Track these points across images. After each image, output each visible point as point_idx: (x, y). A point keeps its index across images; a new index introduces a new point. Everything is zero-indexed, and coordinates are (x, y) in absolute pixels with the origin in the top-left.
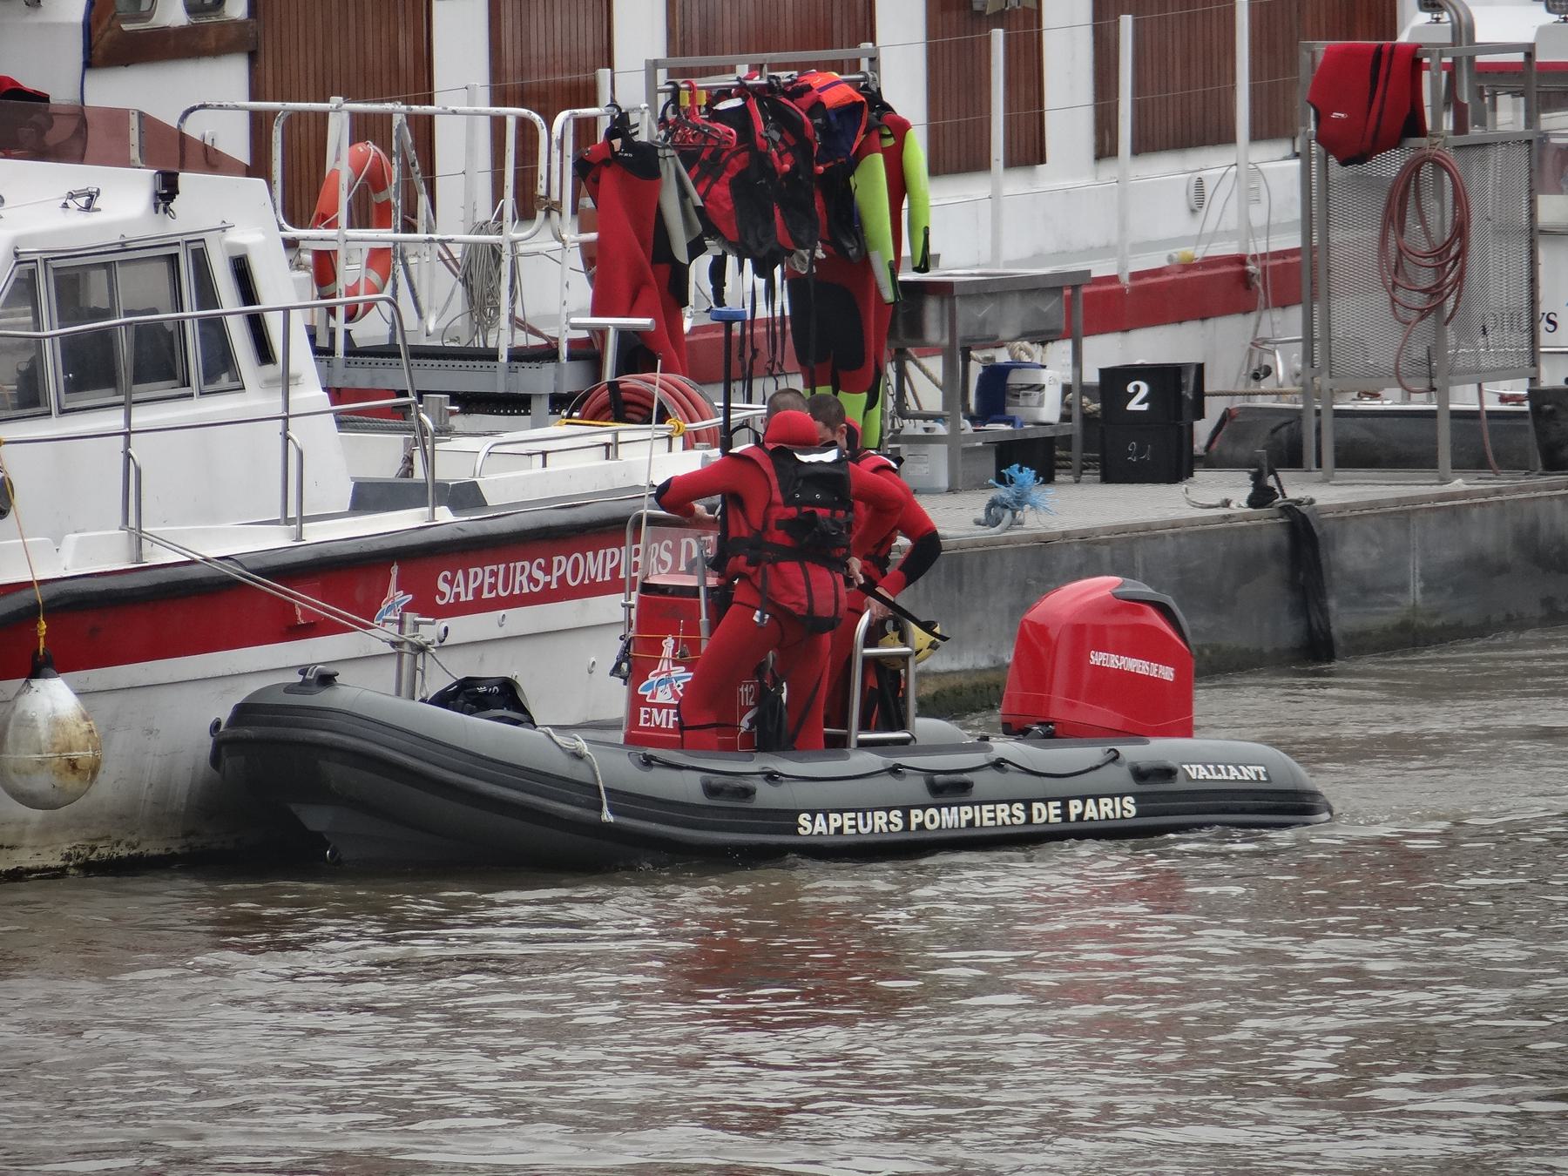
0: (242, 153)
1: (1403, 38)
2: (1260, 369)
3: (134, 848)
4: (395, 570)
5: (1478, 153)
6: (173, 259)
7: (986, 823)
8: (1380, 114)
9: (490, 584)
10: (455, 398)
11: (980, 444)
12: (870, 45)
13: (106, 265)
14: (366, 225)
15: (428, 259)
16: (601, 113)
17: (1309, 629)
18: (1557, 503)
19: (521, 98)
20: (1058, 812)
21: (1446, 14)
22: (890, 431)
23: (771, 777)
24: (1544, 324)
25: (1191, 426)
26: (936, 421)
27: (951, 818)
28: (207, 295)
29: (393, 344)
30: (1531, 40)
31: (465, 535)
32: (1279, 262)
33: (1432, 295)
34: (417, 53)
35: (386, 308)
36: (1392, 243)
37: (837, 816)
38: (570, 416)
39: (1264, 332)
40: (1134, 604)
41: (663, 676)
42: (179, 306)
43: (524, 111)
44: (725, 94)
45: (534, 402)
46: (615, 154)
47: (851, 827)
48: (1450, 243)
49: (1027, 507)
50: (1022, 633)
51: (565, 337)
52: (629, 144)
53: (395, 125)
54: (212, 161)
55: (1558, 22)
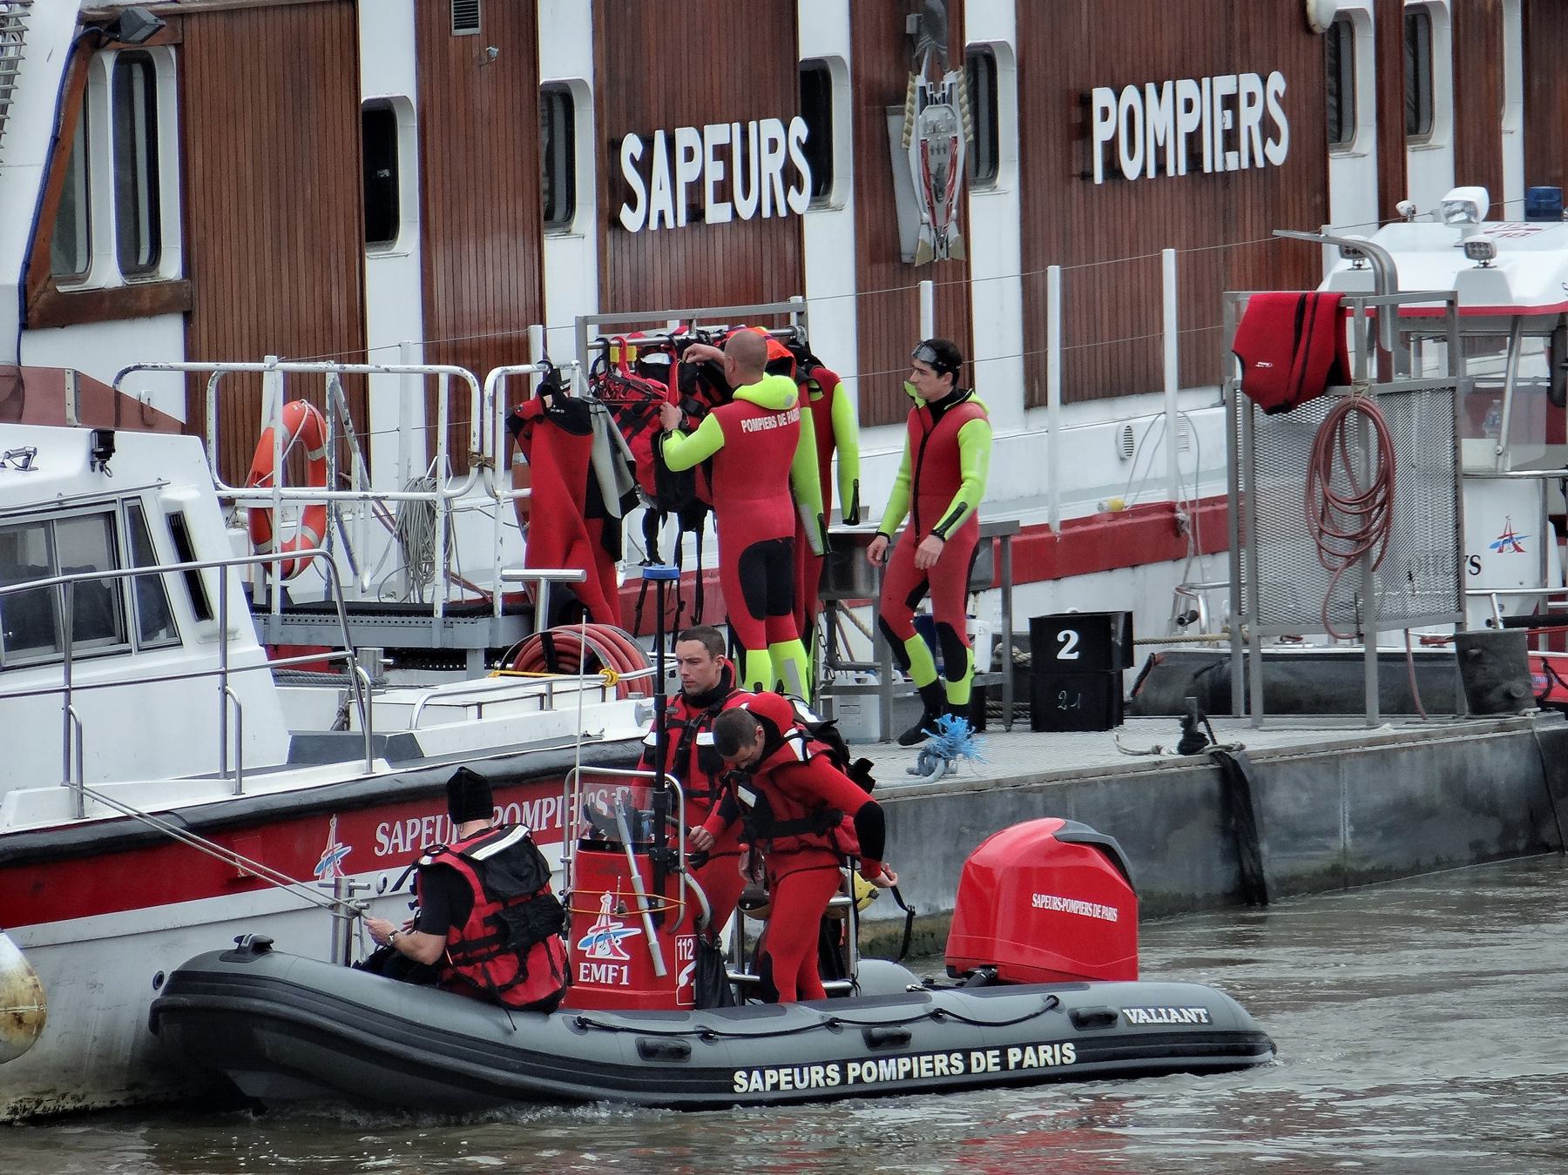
0: (178, 412)
1: (1324, 288)
2: (1186, 614)
3: (79, 1101)
4: (334, 822)
5: (1402, 400)
6: (110, 516)
7: (924, 1074)
8: (1305, 363)
9: (428, 835)
10: (388, 652)
11: (911, 694)
12: (800, 298)
13: (43, 524)
14: (302, 483)
15: (362, 515)
16: (534, 371)
17: (1242, 874)
18: (1485, 746)
19: (454, 355)
20: (997, 1060)
21: (1367, 260)
22: (823, 682)
23: (706, 1036)
24: (1468, 566)
25: (1121, 674)
26: (867, 672)
27: (890, 1070)
28: (144, 552)
29: (329, 601)
30: (1451, 288)
31: (403, 786)
32: (1210, 508)
33: (1359, 541)
34: (350, 311)
35: (321, 562)
36: (1318, 490)
37: (774, 1072)
38: (503, 668)
39: (1194, 578)
40: (1076, 845)
41: (602, 932)
42: (117, 564)
43: (456, 369)
44: (655, 348)
45: (469, 658)
46: (546, 411)
47: (787, 1083)
48: (1376, 489)
49: (960, 756)
50: (966, 875)
51: (500, 591)
52: (560, 400)
53: (328, 384)
54: (147, 419)
55: (1478, 267)
